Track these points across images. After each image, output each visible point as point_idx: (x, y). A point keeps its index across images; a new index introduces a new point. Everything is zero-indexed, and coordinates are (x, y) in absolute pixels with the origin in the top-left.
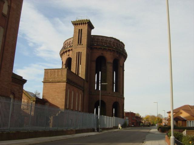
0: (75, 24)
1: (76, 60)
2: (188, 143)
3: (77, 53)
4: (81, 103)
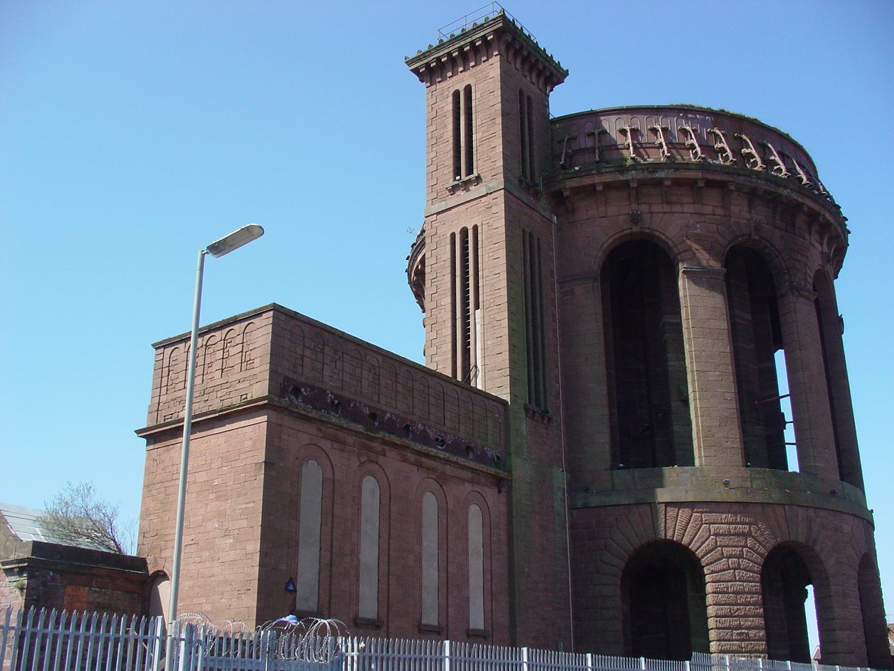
0: (431, 69)
1: (449, 285)
2: (273, 650)
3: (453, 235)
4: (488, 573)
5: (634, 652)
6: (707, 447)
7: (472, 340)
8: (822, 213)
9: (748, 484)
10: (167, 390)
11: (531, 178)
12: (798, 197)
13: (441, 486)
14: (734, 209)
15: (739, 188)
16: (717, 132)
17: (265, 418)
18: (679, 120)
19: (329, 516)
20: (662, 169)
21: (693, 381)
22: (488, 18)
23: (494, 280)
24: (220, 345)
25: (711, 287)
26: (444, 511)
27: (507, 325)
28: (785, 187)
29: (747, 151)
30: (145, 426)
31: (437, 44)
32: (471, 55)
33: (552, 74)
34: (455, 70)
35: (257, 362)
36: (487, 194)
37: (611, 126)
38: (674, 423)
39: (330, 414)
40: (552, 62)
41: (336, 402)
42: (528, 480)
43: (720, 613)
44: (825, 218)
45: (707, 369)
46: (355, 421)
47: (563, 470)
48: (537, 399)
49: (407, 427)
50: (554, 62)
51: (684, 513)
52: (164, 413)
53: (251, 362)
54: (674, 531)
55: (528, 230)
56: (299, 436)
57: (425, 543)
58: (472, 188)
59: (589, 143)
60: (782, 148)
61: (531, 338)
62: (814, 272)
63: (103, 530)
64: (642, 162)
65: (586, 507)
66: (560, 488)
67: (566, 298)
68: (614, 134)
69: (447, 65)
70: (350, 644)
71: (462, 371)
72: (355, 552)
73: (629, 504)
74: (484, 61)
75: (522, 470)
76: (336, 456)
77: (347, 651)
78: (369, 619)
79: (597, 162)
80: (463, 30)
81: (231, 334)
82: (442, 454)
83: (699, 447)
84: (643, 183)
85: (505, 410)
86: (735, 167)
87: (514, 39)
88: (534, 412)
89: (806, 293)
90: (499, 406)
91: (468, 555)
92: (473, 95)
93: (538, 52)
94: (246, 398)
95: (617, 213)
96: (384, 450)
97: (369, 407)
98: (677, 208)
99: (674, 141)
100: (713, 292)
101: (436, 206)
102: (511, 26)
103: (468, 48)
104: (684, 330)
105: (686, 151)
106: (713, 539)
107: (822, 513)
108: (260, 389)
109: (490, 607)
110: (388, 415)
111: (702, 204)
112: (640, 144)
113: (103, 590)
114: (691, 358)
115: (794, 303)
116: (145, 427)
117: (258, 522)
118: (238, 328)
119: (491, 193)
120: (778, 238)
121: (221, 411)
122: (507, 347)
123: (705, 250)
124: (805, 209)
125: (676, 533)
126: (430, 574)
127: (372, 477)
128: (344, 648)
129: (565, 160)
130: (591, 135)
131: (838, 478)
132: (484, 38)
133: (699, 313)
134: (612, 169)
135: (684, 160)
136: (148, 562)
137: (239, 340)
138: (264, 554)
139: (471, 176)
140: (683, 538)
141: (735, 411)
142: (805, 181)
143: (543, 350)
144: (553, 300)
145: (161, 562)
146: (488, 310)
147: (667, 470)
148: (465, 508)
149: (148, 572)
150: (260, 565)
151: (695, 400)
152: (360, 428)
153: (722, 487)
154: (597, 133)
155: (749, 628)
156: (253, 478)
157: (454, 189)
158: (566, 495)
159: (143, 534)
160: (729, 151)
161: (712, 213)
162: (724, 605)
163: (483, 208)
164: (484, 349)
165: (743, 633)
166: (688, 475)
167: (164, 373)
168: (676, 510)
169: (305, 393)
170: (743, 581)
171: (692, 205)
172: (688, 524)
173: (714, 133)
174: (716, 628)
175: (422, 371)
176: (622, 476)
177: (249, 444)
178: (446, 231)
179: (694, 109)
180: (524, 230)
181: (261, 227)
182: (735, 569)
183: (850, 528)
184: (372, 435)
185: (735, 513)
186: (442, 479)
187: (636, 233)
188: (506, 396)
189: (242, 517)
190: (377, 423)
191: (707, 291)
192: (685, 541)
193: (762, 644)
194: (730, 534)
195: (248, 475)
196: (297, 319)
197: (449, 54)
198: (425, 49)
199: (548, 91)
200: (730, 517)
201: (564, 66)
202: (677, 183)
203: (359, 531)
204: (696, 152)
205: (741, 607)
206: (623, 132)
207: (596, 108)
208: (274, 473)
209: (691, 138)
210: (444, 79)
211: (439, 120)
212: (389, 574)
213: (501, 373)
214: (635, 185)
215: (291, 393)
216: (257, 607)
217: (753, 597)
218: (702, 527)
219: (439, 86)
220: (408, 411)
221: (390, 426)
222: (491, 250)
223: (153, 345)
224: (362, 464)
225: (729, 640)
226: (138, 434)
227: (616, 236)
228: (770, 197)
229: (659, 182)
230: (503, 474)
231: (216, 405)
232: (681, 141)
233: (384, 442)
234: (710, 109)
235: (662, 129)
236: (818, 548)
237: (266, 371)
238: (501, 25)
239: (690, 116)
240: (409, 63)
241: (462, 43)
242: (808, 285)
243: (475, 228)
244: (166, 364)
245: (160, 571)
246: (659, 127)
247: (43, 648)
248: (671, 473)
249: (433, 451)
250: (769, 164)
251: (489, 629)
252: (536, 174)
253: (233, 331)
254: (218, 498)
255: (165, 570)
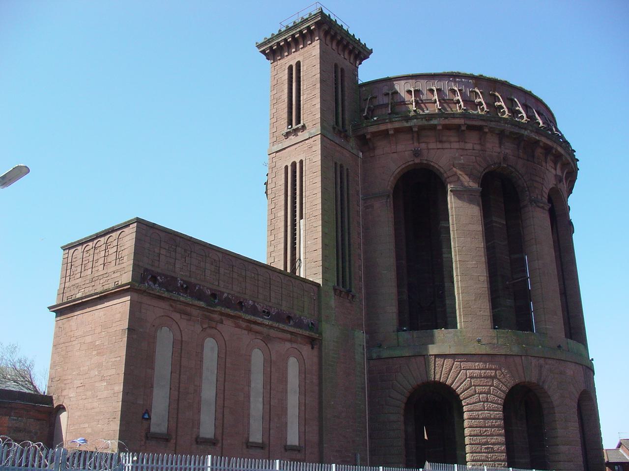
0: (274, 50)
1: (283, 202)
3: (286, 167)
4: (303, 407)
5: (375, 464)
6: (465, 315)
7: (297, 241)
8: (555, 147)
9: (495, 341)
10: (70, 279)
12: (535, 136)
13: (266, 344)
14: (489, 146)
15: (492, 130)
16: (477, 91)
17: (129, 298)
18: (450, 83)
19: (177, 367)
20: (435, 118)
21: (457, 268)
22: (310, 14)
23: (313, 199)
24: (103, 247)
25: (470, 201)
26: (269, 363)
27: (321, 230)
28: (526, 129)
29: (499, 104)
30: (55, 303)
31: (277, 33)
32: (300, 40)
33: (360, 52)
34: (290, 50)
35: (125, 258)
36: (309, 138)
37: (401, 88)
38: (447, 298)
39: (180, 295)
40: (359, 44)
41: (185, 286)
42: (335, 340)
43: (472, 433)
44: (556, 150)
45: (466, 260)
46: (199, 299)
47: (363, 332)
49: (241, 303)
50: (361, 43)
51: (448, 362)
52: (67, 295)
53: (122, 258)
54: (441, 375)
55: (339, 163)
56: (155, 311)
57: (253, 385)
58: (300, 134)
59: (386, 100)
60: (526, 101)
61: (340, 239)
62: (549, 190)
63: (25, 376)
64: (421, 112)
65: (379, 358)
66: (360, 345)
67: (367, 210)
68: (403, 94)
69: (284, 48)
70: (127, 458)
71: (291, 263)
72: (198, 391)
73: (409, 356)
74: (309, 44)
75: (330, 333)
76: (183, 324)
77: (126, 463)
78: (209, 439)
79: (389, 114)
80: (294, 22)
82: (267, 322)
83: (460, 315)
84: (422, 128)
85: (318, 290)
86: (488, 115)
87: (330, 28)
88: (341, 292)
89: (542, 205)
90: (314, 287)
91: (287, 392)
92: (301, 68)
93: (349, 37)
94: (118, 284)
95: (404, 150)
96: (222, 319)
97: (211, 289)
98: (447, 145)
99: (445, 98)
100: (472, 205)
101: (275, 146)
102: (327, 19)
103: (298, 35)
104: (451, 232)
105: (455, 105)
106: (468, 381)
107: (550, 362)
108: (126, 278)
109: (304, 430)
110: (225, 295)
111: (465, 142)
112: (421, 100)
113: (19, 418)
114: (455, 252)
115: (532, 211)
116: (55, 304)
117: (122, 371)
118: (115, 235)
119: (312, 137)
120: (519, 164)
121: (101, 293)
122: (320, 246)
123: (466, 174)
124: (541, 144)
125: (442, 377)
126: (257, 407)
127: (211, 339)
128: (124, 460)
129: (367, 113)
130: (387, 94)
131: (564, 336)
132: (308, 28)
133: (462, 220)
134: (400, 119)
135: (452, 111)
136: (54, 399)
137: (115, 243)
138: (125, 393)
139: (299, 125)
140: (447, 380)
141: (487, 289)
142: (541, 124)
143: (349, 247)
144: (358, 212)
145: (61, 399)
146: (309, 219)
147: (437, 332)
148: (285, 361)
149: (53, 405)
150: (123, 401)
151: (457, 281)
152: (202, 304)
153: (476, 344)
154: (390, 93)
155: (494, 444)
156: (121, 340)
157: (287, 135)
158: (365, 350)
159: (51, 379)
160: (484, 104)
161: (426, 148)
162: (476, 427)
163: (307, 148)
164: (305, 247)
165: (490, 447)
166: (452, 335)
167: (68, 265)
168: (443, 360)
169: (160, 280)
170: (490, 411)
171: (458, 143)
172: (451, 370)
173: (475, 91)
174: (470, 444)
175: (253, 263)
176: (405, 336)
177: (118, 316)
178: (282, 164)
179: (460, 75)
180: (336, 163)
181: (26, 167)
182: (484, 402)
183: (572, 372)
184: (212, 309)
185: (485, 362)
186: (267, 339)
188: (319, 281)
189: (113, 367)
190: (216, 301)
191: (468, 205)
192: (448, 382)
193: (503, 456)
194: (481, 377)
195: (117, 337)
196: (154, 228)
197: (285, 40)
198: (269, 37)
199: (357, 64)
200: (481, 365)
201: (369, 47)
202: (447, 127)
203: (201, 377)
204: (483, 107)
205: (489, 429)
206: (409, 92)
207: (391, 75)
208: (135, 336)
209: (458, 96)
210: (282, 57)
211: (279, 87)
212: (224, 407)
213: (316, 264)
214: (417, 130)
215: (150, 280)
216: (120, 430)
217: (497, 422)
218: (461, 372)
219: (279, 62)
220: (241, 291)
221: (227, 303)
222: (312, 178)
223: (62, 248)
224: (204, 329)
225: (479, 453)
226: (50, 309)
227: (404, 166)
228: (515, 136)
229: (433, 128)
230: (316, 336)
231: (99, 289)
232: (451, 98)
233: (222, 314)
234: (472, 74)
235: (437, 90)
236: (547, 387)
237: (131, 265)
238: (320, 18)
239: (457, 80)
240: (259, 46)
241: (294, 32)
242: (543, 198)
243: (301, 162)
244: (70, 261)
245: (61, 405)
246: (434, 88)
248: (440, 334)
249: (260, 320)
250: (515, 113)
251: (303, 445)
252: (347, 122)
253: (111, 237)
254: (98, 354)
255: (64, 404)
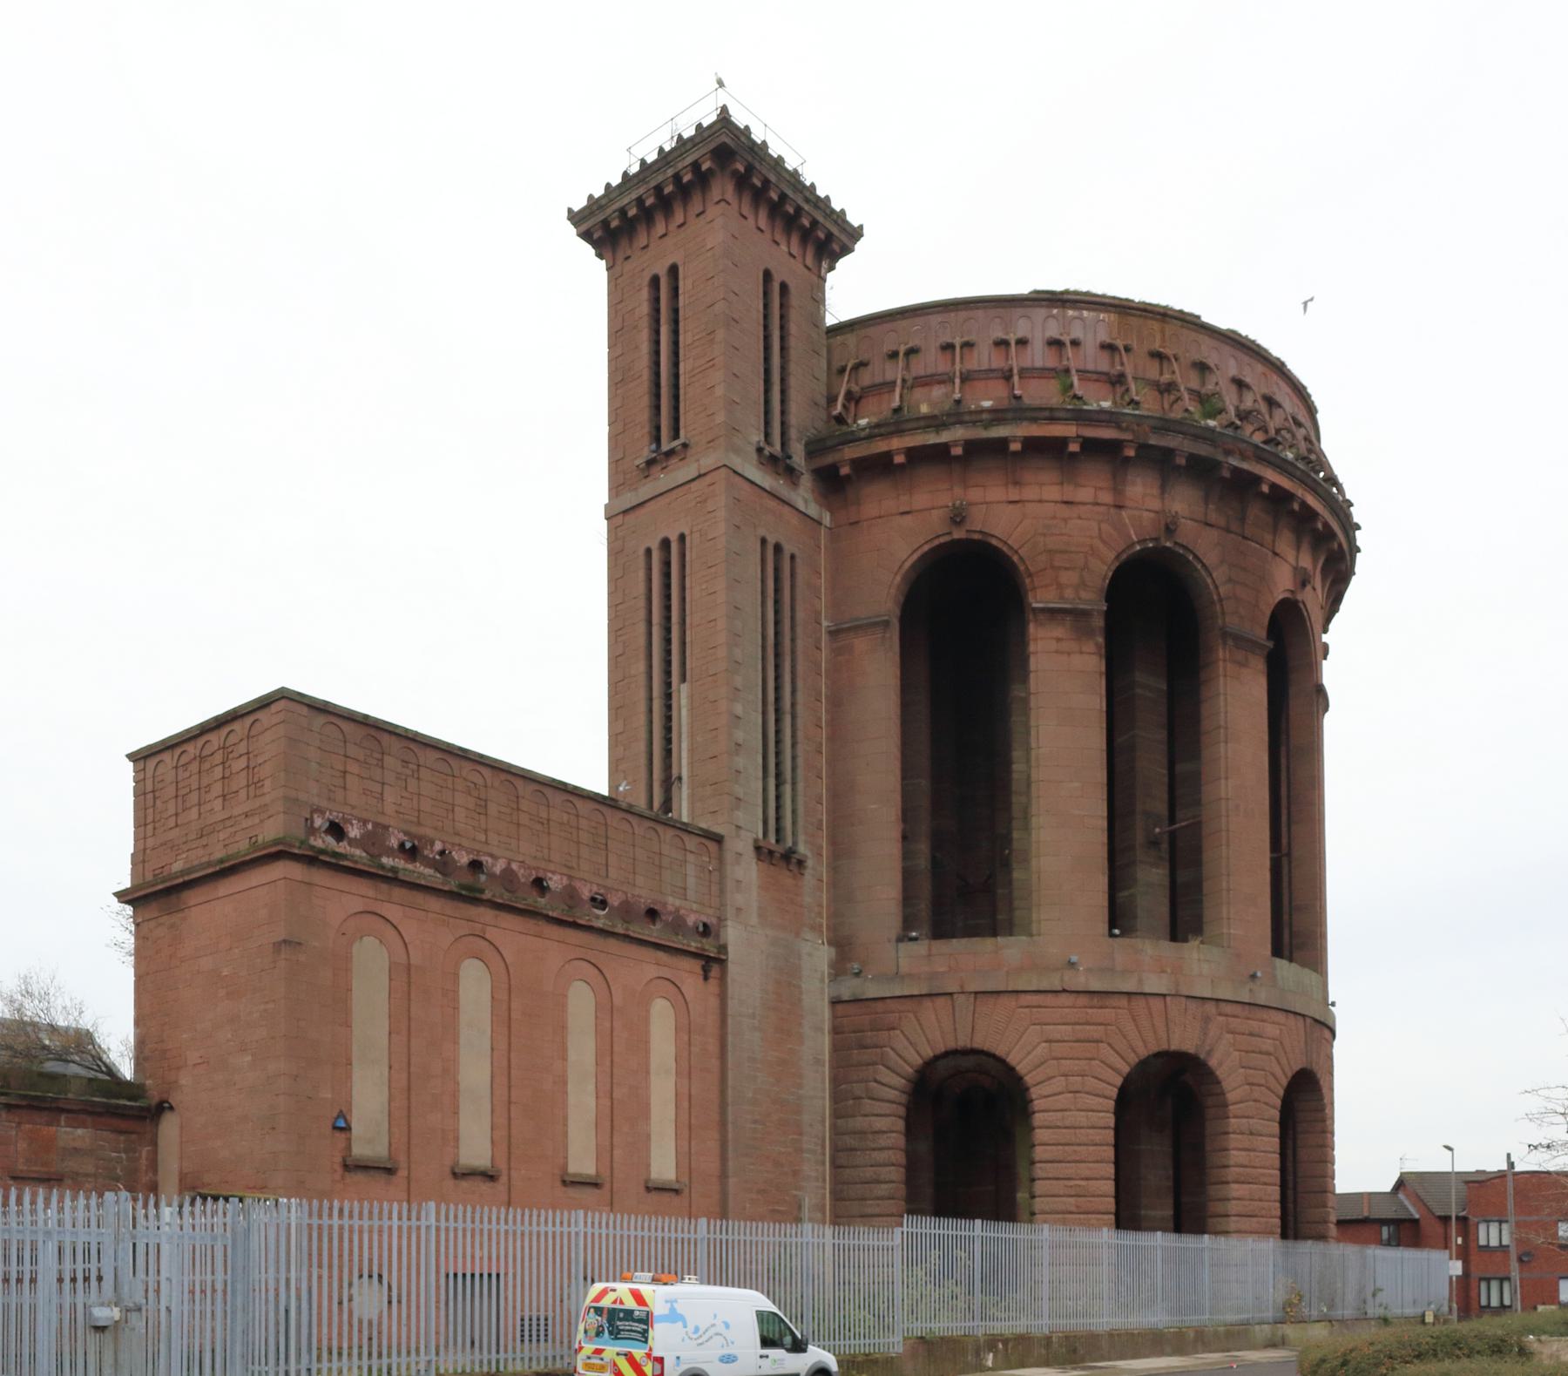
3: (649, 552)
4: (685, 1102)
11: (783, 444)
24: (218, 757)
36: (700, 476)
41: (408, 845)
48: (779, 830)
55: (771, 540)
57: (572, 1056)
63: (81, 1043)
72: (450, 1071)
81: (232, 739)
91: (648, 1072)
129: (844, 406)
132: (696, 166)
187: (959, 541)
201: (854, 219)
220: (539, 854)
231: (219, 854)
243: (682, 538)
247: (351, 1241)
251: (685, 1180)
